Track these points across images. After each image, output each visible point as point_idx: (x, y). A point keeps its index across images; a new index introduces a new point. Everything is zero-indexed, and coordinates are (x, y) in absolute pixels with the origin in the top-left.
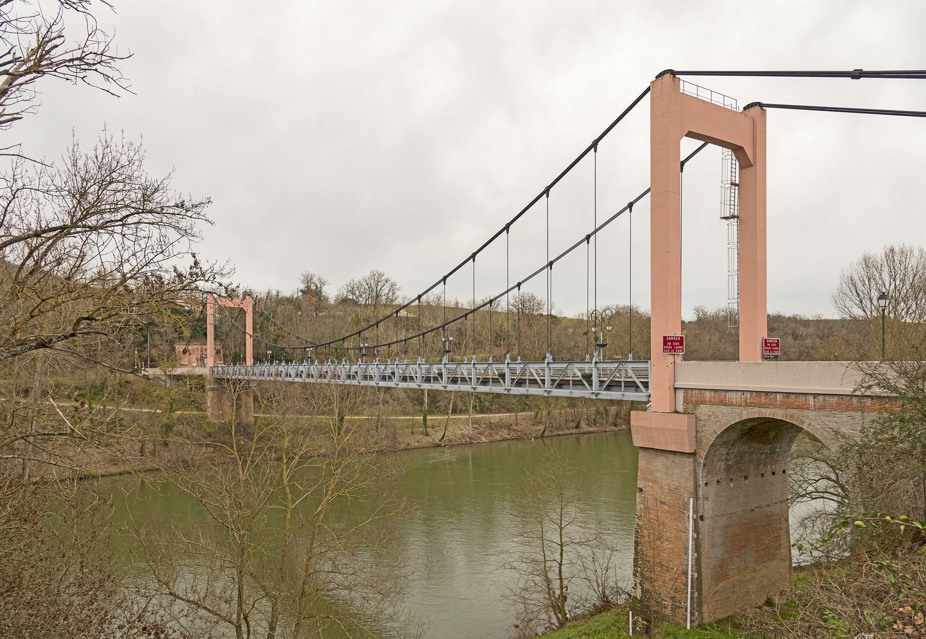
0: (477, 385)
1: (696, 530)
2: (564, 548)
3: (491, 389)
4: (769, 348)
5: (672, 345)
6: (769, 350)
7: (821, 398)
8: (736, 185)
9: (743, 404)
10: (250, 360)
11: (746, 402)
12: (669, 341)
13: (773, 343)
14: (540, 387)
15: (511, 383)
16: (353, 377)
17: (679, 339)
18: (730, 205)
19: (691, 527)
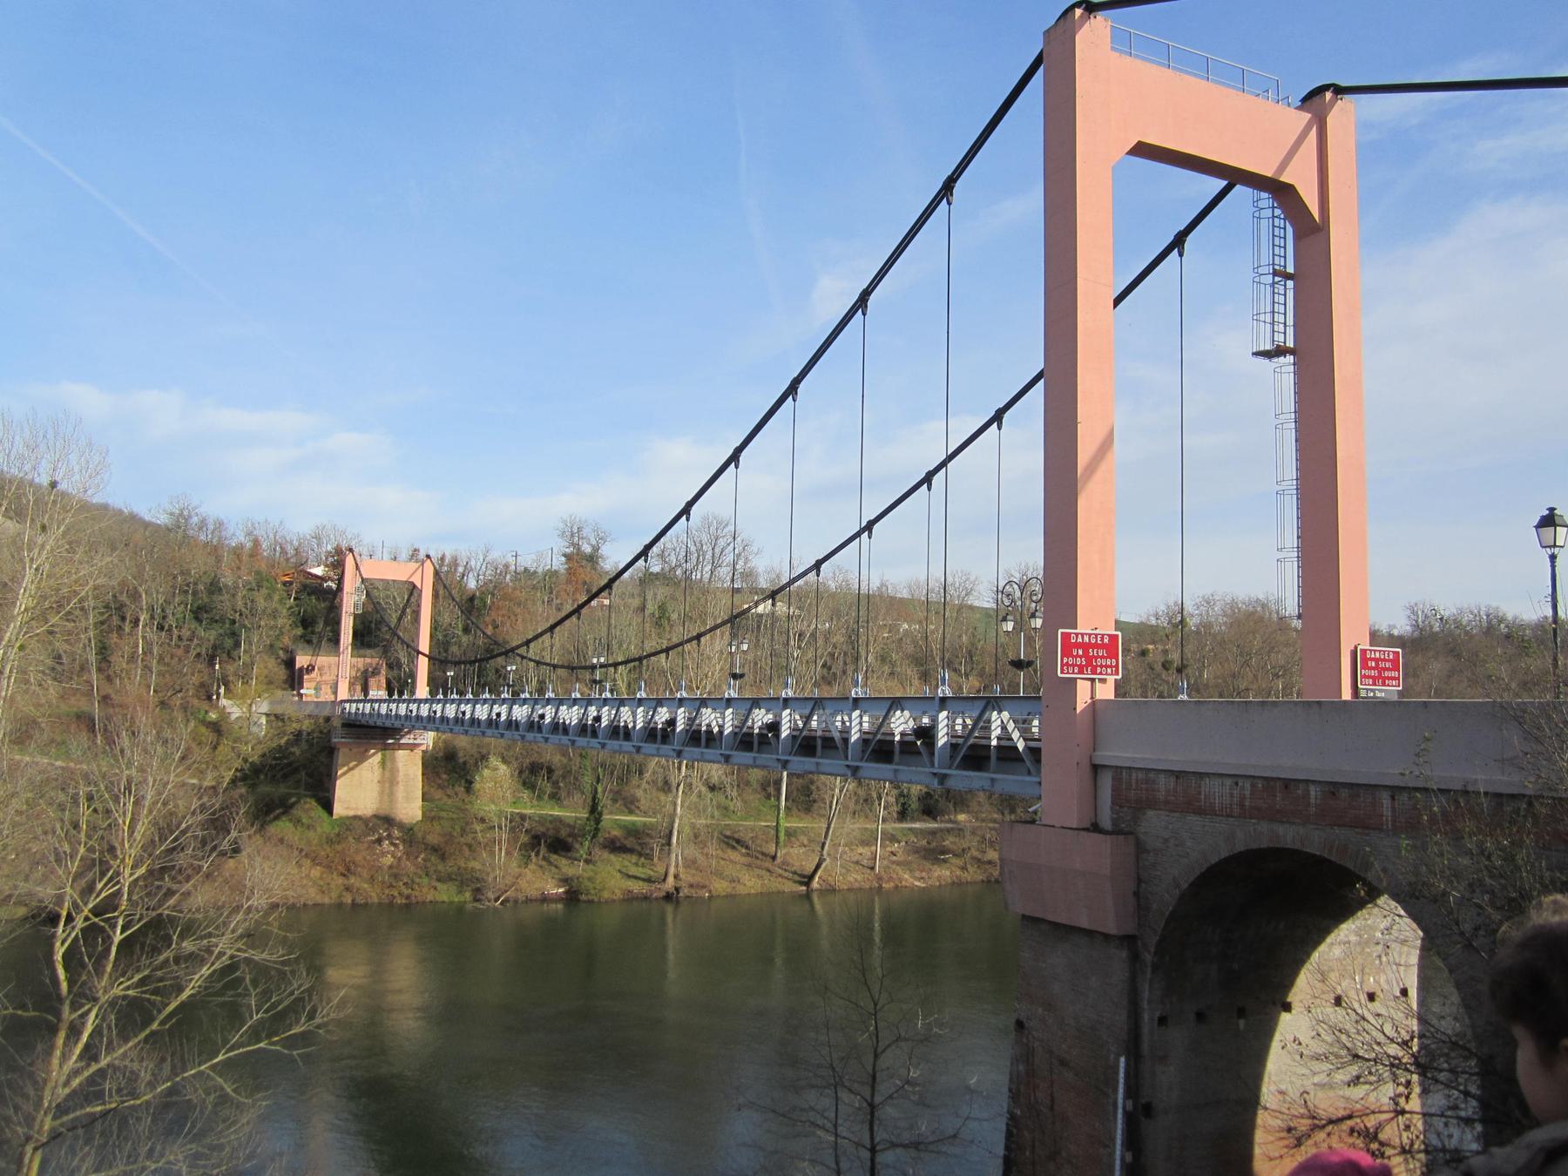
0: (862, 760)
1: (1133, 1140)
2: (880, 1158)
3: (755, 758)
4: (1373, 673)
5: (1086, 654)
6: (1374, 678)
7: (1404, 797)
8: (1288, 277)
9: (1236, 811)
10: (422, 691)
11: (1242, 805)
12: (1077, 646)
13: (1384, 660)
14: (1029, 773)
15: (951, 757)
16: (760, 743)
17: (1106, 641)
18: (1273, 323)
19: (1119, 1132)
